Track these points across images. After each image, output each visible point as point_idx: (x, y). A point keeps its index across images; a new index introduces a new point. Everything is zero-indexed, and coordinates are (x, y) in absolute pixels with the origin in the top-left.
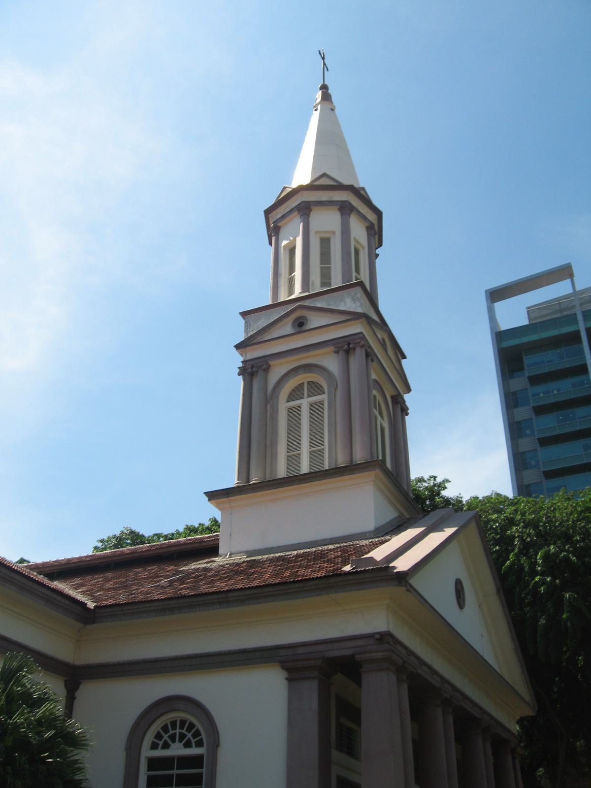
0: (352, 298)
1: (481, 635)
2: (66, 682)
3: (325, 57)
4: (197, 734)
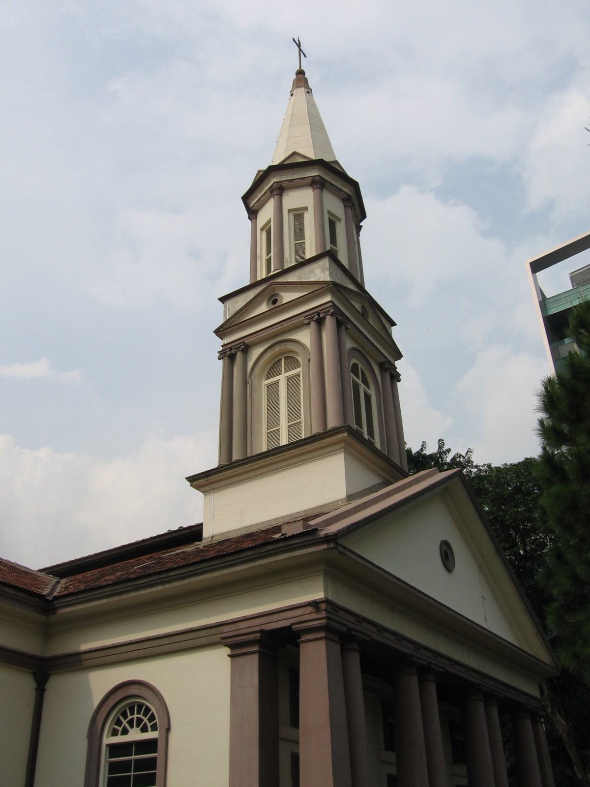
0: (322, 268)
1: (483, 597)
4: (152, 718)
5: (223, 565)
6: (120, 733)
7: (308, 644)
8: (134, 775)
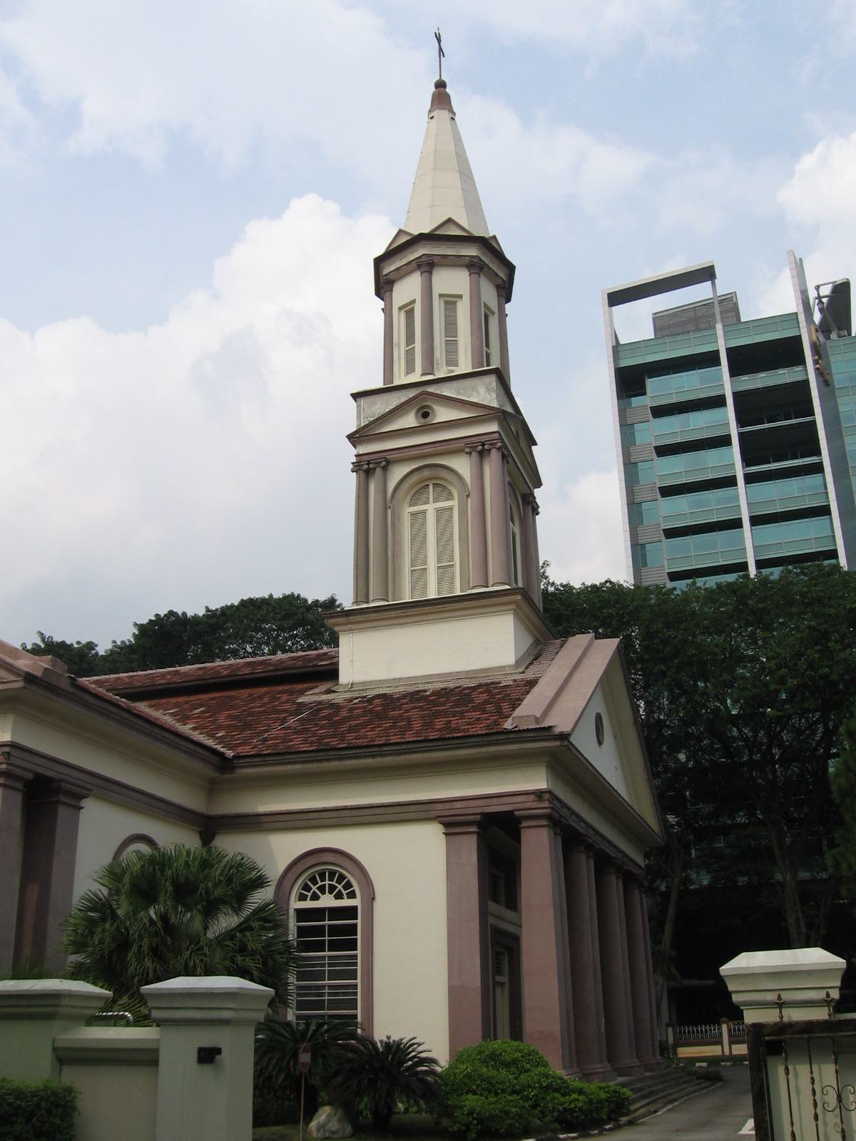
0: (487, 387)
2: (201, 833)
3: (441, 38)
4: (348, 885)
5: (447, 747)
6: (309, 898)
7: (529, 830)
8: (328, 940)
